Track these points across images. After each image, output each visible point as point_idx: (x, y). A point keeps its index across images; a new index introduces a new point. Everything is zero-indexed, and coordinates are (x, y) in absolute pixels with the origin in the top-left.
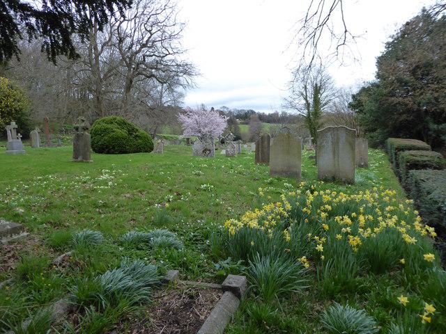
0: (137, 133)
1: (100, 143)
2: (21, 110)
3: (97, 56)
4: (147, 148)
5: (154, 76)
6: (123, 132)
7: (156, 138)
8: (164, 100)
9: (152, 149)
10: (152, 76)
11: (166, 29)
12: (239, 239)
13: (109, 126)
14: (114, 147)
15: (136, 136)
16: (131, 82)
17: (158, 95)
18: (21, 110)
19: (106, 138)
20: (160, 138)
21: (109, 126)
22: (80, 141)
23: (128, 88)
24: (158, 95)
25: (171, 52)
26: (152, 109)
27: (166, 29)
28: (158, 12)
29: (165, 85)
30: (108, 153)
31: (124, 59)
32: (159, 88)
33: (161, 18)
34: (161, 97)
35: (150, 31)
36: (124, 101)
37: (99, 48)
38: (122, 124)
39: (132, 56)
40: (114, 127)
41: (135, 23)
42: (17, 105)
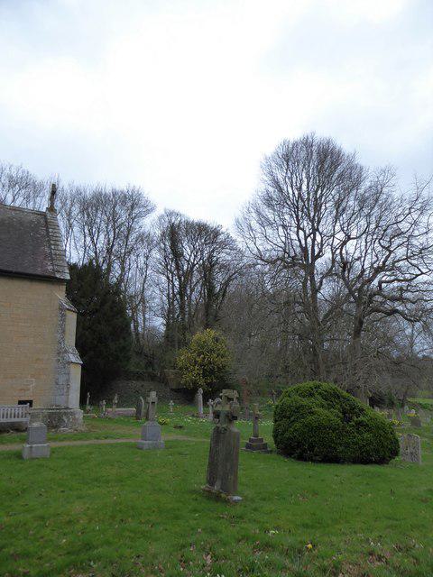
0: (361, 418)
1: (287, 435)
2: (224, 367)
3: (316, 290)
4: (380, 450)
5: (397, 311)
6: (330, 415)
7: (406, 408)
8: (417, 348)
9: (395, 453)
10: (395, 311)
11: (414, 242)
12: (291, 146)
13: (305, 402)
14: (311, 448)
15: (360, 424)
16: (361, 323)
17: (407, 342)
18: (224, 367)
19: (297, 425)
20: (414, 406)
21: (305, 402)
22: (221, 444)
23: (357, 333)
24: (407, 342)
25: (424, 271)
26: (397, 363)
27: (414, 242)
28: (399, 219)
29: (418, 325)
30: (301, 458)
31: (351, 293)
32: (409, 331)
33: (404, 226)
34: (412, 344)
35: (387, 249)
36: (352, 348)
37: (317, 279)
38: (331, 397)
39: (363, 285)
40: (314, 403)
41: (366, 242)
42: (220, 361)
